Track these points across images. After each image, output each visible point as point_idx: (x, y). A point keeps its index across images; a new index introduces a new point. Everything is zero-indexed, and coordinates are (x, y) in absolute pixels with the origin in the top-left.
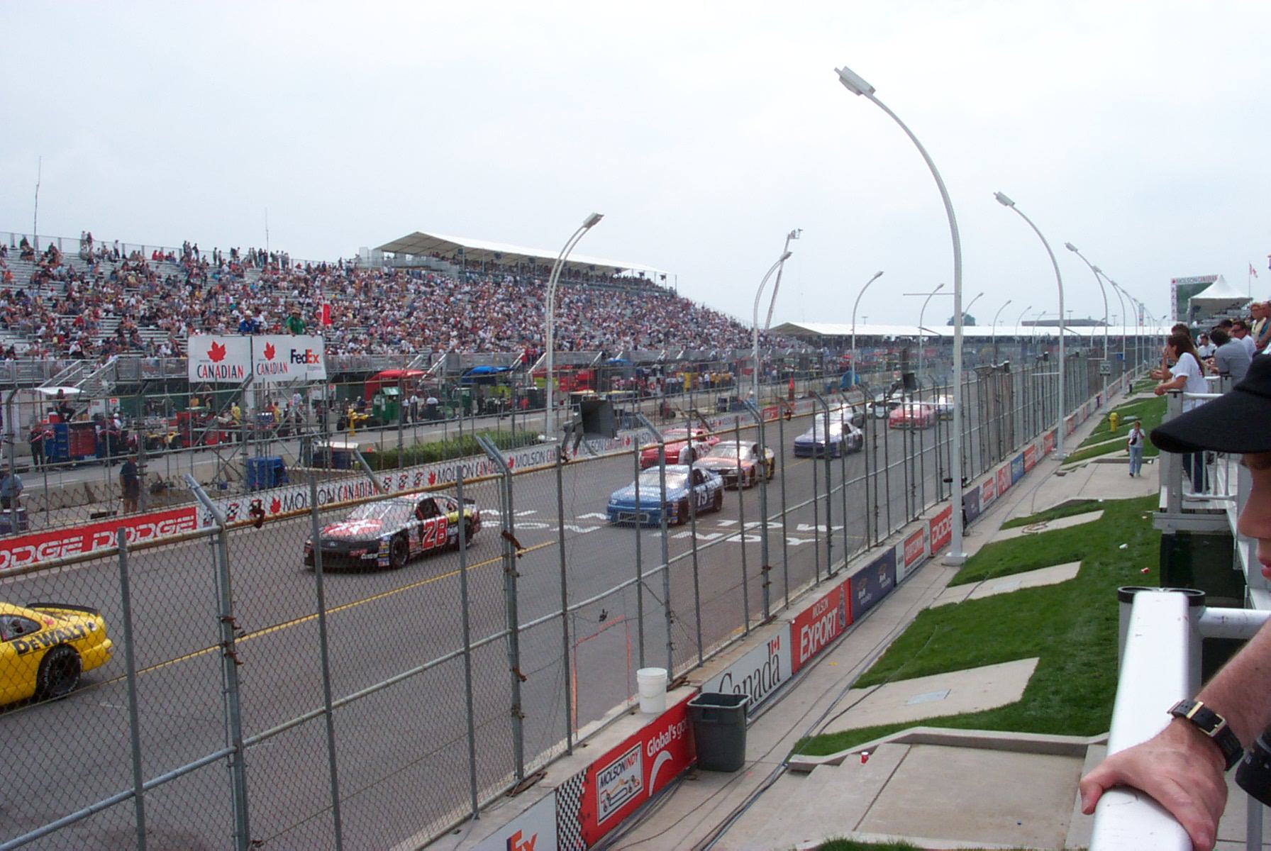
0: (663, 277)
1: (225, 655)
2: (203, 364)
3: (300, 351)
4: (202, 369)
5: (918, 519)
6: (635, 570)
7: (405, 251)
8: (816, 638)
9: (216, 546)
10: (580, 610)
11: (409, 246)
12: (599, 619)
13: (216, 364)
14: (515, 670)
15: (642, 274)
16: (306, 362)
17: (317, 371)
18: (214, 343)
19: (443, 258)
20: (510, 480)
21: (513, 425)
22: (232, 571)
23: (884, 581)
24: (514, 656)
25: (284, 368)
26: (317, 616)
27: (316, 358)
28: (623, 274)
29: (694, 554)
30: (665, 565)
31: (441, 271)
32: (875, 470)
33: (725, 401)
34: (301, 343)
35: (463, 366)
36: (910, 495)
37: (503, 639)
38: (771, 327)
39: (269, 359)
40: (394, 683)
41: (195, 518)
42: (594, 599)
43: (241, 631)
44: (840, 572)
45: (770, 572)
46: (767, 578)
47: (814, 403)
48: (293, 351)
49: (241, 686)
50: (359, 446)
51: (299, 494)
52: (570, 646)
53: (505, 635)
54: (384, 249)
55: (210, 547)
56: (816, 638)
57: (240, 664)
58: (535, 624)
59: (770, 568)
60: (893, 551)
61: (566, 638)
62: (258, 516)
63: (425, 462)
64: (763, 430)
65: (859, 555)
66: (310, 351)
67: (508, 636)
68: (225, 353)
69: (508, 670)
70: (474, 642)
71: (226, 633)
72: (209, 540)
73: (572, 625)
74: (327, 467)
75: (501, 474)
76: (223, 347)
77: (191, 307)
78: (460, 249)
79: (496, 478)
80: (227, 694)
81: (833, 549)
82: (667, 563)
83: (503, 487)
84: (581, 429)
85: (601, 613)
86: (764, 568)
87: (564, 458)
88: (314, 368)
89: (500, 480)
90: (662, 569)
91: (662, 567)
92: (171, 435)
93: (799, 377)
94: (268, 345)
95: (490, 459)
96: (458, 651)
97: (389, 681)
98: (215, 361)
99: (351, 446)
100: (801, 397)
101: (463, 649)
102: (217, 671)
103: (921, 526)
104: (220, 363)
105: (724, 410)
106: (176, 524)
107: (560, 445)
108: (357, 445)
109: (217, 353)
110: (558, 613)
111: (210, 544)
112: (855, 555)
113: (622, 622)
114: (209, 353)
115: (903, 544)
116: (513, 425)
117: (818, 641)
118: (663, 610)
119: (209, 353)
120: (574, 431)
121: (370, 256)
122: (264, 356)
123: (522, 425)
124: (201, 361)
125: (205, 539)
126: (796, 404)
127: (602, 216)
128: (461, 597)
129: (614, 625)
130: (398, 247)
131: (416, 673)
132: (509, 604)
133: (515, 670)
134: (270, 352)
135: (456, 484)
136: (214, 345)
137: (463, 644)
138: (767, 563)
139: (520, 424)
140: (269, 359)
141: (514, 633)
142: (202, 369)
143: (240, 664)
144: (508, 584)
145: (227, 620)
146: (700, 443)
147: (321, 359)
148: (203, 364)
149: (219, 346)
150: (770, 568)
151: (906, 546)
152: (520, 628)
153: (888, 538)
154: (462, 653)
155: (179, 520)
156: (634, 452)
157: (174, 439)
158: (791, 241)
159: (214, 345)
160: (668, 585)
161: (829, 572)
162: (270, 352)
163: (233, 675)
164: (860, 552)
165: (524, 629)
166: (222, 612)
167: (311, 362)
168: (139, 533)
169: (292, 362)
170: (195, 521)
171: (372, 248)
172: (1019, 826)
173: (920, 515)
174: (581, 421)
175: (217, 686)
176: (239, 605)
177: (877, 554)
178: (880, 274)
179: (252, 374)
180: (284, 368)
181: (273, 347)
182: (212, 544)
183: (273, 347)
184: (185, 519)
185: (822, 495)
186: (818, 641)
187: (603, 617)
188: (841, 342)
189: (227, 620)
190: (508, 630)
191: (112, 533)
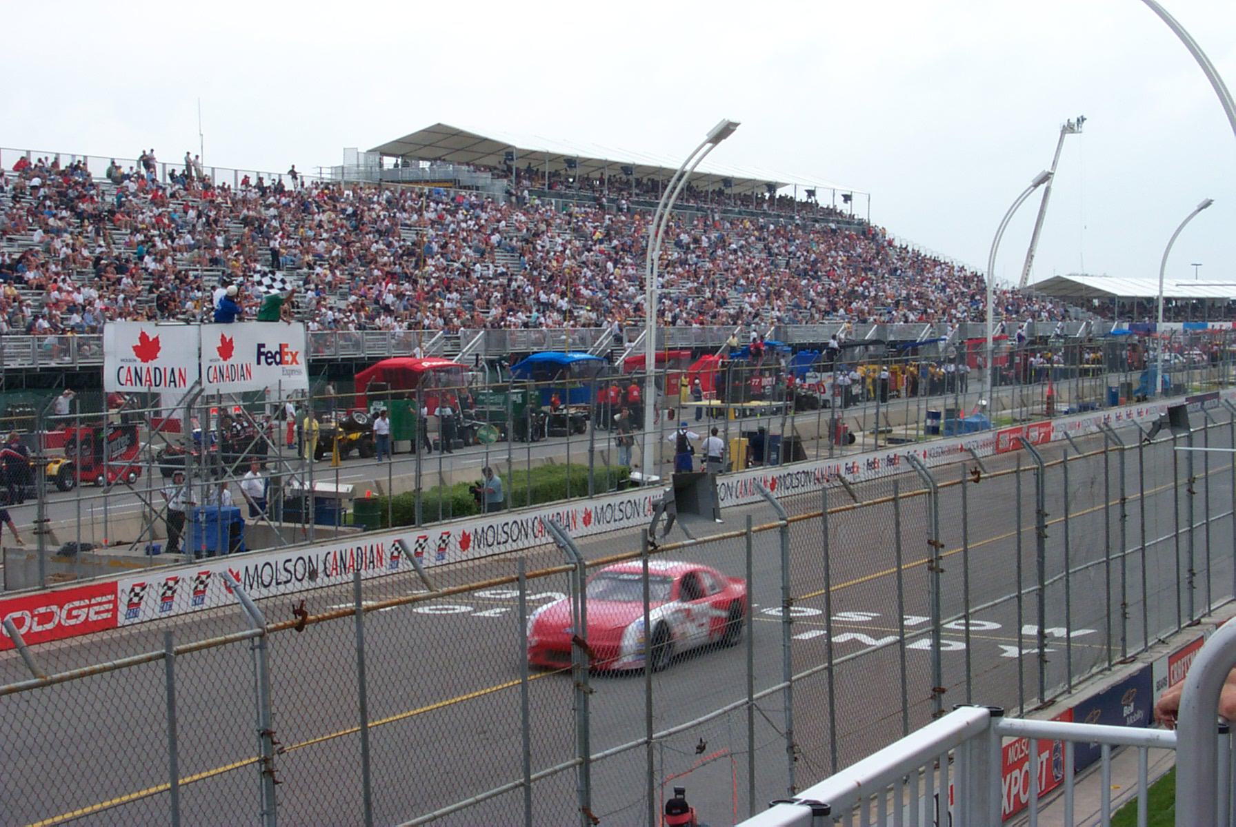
0: (847, 198)
1: (264, 773)
2: (126, 365)
3: (272, 347)
4: (123, 373)
5: (1198, 623)
6: (745, 687)
7: (422, 153)
8: (1014, 791)
9: (257, 651)
10: (669, 738)
11: (425, 146)
12: (695, 750)
13: (145, 366)
14: (586, 810)
15: (811, 193)
16: (280, 363)
17: (294, 377)
18: (143, 334)
19: (477, 169)
20: (583, 573)
21: (592, 451)
22: (272, 678)
23: (1132, 714)
24: (585, 792)
25: (246, 372)
26: (180, 782)
27: (294, 356)
28: (780, 192)
29: (830, 669)
30: (787, 683)
31: (477, 188)
32: (1123, 549)
33: (936, 416)
34: (274, 334)
35: (511, 350)
36: (1184, 585)
37: (571, 770)
38: (1029, 283)
39: (225, 359)
40: (441, 816)
41: (116, 597)
42: (688, 724)
43: (279, 746)
44: (1058, 700)
45: (944, 697)
46: (940, 705)
47: (1019, 455)
48: (261, 346)
49: (278, 808)
50: (353, 489)
51: (300, 580)
52: (656, 785)
53: (573, 766)
54: (384, 151)
55: (251, 652)
56: (1014, 791)
57: (277, 783)
58: (611, 754)
59: (943, 691)
60: (1148, 671)
61: (651, 773)
62: (300, 618)
63: (455, 516)
64: (936, 497)
65: (1093, 676)
66: (287, 346)
67: (577, 766)
68: (159, 349)
69: (576, 810)
70: (536, 771)
71: (265, 747)
72: (251, 645)
73: (659, 756)
74: (307, 523)
75: (573, 566)
76: (156, 340)
77: (74, 250)
78: (508, 152)
79: (566, 571)
80: (265, 816)
81: (1047, 666)
82: (790, 680)
83: (574, 580)
84: (673, 509)
85: (698, 743)
86: (934, 690)
87: (652, 544)
88: (293, 372)
89: (570, 573)
90: (783, 688)
91: (782, 685)
92: (57, 462)
93: (1064, 374)
94: (223, 338)
95: (558, 546)
96: (517, 782)
97: (436, 813)
98: (145, 360)
99: (343, 488)
100: (1065, 408)
101: (522, 780)
102: (255, 789)
103: (1201, 634)
104: (152, 364)
105: (934, 431)
106: (89, 606)
107: (648, 527)
108: (351, 487)
109: (148, 349)
110: (640, 740)
111: (251, 649)
112: (1087, 676)
113: (726, 756)
114: (135, 348)
115: (1166, 659)
116: (592, 451)
117: (1017, 796)
118: (784, 743)
119: (135, 348)
120: (665, 510)
121: (362, 162)
122: (218, 353)
123: (605, 454)
124: (122, 360)
125: (246, 642)
126: (1054, 423)
127: (737, 125)
128: (521, 716)
129: (715, 760)
130: (407, 149)
131: (466, 806)
132: (579, 726)
133: (586, 810)
134: (226, 349)
135: (518, 579)
136: (144, 337)
137: (522, 775)
138: (939, 683)
139: (602, 452)
140: (225, 359)
141: (585, 764)
142: (123, 373)
143: (277, 783)
144: (579, 703)
145: (266, 734)
146: (686, 605)
147: (301, 359)
148: (126, 365)
149: (151, 339)
150: (943, 691)
151: (1171, 663)
152: (592, 757)
153: (1145, 650)
154: (522, 785)
155: (93, 601)
156: (746, 534)
157: (61, 469)
158: (1068, 136)
159: (144, 337)
160: (790, 710)
161: (1042, 700)
162: (226, 349)
163: (271, 795)
164: (1095, 670)
165: (597, 759)
166: (261, 725)
167: (287, 363)
168: (36, 619)
169: (259, 363)
170: (115, 602)
171: (363, 149)
172: (708, 753)
173: (1204, 616)
174: (673, 498)
175: (255, 806)
176: (278, 717)
177: (1121, 673)
178: (1208, 204)
179: (199, 382)
180: (246, 372)
181: (231, 340)
182: (253, 649)
183: (231, 340)
184: (99, 599)
185: (1030, 588)
186: (1017, 796)
187: (701, 749)
188: (1141, 308)
189: (266, 734)
190: (578, 759)
191: (63, 622)
